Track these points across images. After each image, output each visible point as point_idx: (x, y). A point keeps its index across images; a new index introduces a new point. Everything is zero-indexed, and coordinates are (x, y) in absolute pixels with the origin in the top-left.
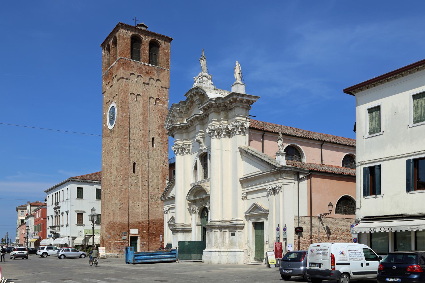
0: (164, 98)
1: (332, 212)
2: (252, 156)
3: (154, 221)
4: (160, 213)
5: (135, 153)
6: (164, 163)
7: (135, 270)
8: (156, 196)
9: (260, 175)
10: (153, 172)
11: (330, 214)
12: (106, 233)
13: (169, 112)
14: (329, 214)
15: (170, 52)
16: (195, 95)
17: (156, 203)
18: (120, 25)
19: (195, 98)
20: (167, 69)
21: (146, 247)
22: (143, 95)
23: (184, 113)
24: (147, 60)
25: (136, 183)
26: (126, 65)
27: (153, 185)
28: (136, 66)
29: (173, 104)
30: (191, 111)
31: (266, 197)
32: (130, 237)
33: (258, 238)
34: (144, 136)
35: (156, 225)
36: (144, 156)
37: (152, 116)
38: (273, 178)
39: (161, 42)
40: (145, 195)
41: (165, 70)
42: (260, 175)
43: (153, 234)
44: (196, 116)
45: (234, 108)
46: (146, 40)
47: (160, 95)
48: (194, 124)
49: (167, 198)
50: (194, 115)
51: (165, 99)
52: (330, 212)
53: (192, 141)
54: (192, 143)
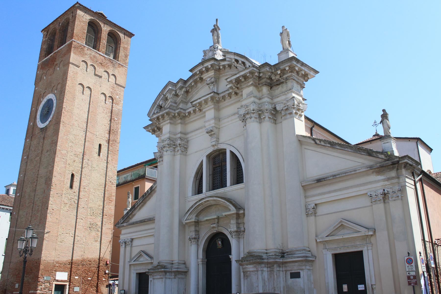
0: (118, 97)
2: (329, 146)
5: (75, 161)
6: (110, 179)
12: (11, 278)
16: (207, 70)
18: (77, 5)
19: (206, 74)
20: (124, 65)
22: (93, 89)
23: (181, 96)
24: (104, 50)
25: (72, 203)
26: (80, 49)
27: (94, 209)
28: (90, 54)
32: (54, 285)
34: (89, 140)
36: (86, 166)
37: (101, 116)
39: (122, 35)
46: (105, 29)
47: (114, 94)
48: (203, 109)
51: (119, 99)
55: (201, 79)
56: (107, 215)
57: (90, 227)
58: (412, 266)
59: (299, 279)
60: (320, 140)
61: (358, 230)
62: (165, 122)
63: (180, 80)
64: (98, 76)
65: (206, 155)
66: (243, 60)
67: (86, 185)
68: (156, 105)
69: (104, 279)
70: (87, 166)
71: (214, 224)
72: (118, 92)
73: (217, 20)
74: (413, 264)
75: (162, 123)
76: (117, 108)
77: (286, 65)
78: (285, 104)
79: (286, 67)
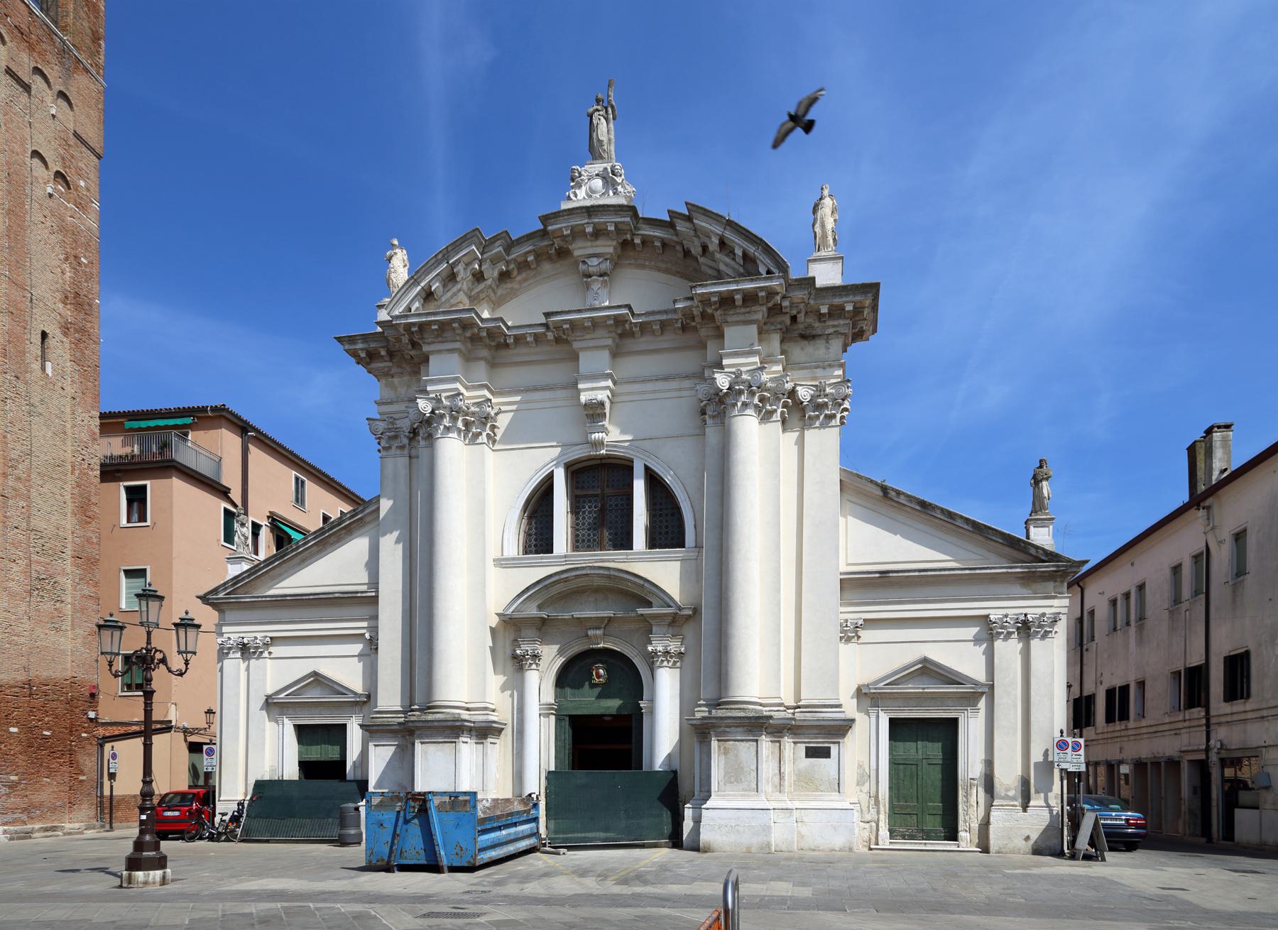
1: (212, 726)
3: (47, 687)
4: (69, 653)
6: (83, 452)
7: (1018, 869)
8: (55, 582)
9: (917, 574)
10: (46, 478)
11: (208, 730)
13: (440, 256)
14: (205, 729)
15: (103, 8)
16: (598, 233)
17: (56, 609)
19: (589, 244)
20: (94, 72)
21: (19, 795)
29: (477, 232)
30: (512, 289)
31: (973, 643)
33: (905, 768)
34: (11, 309)
35: (54, 705)
38: (1017, 589)
40: (16, 568)
41: (87, 71)
42: (917, 574)
43: (42, 739)
44: (625, 311)
45: (825, 337)
49: (254, 597)
50: (619, 307)
52: (210, 726)
53: (518, 398)
54: (514, 407)
55: (563, 253)
56: (81, 558)
57: (37, 589)
59: (828, 759)
60: (899, 493)
62: (445, 344)
63: (504, 235)
64: (15, 79)
65: (565, 461)
66: (751, 249)
67: (16, 457)
68: (419, 288)
69: (84, 735)
70: (16, 397)
71: (599, 628)
72: (80, 164)
75: (429, 343)
76: (85, 225)
77: (851, 298)
78: (820, 391)
79: (847, 302)
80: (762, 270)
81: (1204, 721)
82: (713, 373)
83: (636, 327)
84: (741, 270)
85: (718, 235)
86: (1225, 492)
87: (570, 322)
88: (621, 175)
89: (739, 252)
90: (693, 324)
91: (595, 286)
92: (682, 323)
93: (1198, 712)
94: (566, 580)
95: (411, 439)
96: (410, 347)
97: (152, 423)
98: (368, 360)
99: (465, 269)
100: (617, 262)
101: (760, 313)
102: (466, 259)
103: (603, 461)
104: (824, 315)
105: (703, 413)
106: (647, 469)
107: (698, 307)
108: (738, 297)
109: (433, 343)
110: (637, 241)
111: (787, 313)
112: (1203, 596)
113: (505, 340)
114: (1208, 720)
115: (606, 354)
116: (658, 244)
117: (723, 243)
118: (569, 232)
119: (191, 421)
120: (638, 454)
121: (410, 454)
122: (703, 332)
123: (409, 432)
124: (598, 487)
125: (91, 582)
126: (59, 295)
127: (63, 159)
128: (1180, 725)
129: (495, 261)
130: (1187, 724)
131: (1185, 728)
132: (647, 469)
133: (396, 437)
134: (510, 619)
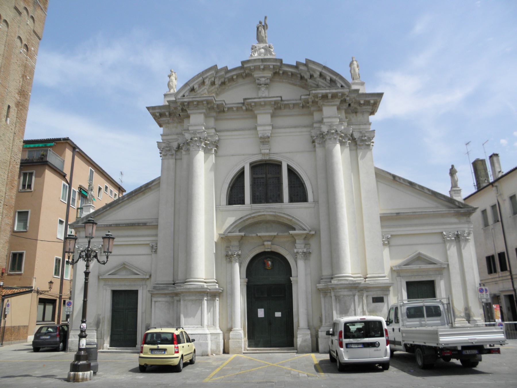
2: (409, 185)
19: (261, 72)
41: (42, 9)
58: (483, 294)
61: (428, 261)
73: (266, 18)
74: (71, 306)
75: (191, 110)
77: (373, 98)
80: (339, 85)
81: (510, 277)
82: (321, 125)
83: (282, 105)
84: (329, 85)
85: (319, 71)
86: (501, 180)
87: (255, 103)
88: (272, 48)
89: (328, 78)
90: (308, 105)
91: (263, 89)
92: (303, 105)
93: (507, 273)
94: (254, 217)
95: (176, 151)
96: (181, 111)
97: (37, 145)
98: (159, 117)
99: (208, 81)
100: (272, 80)
101: (337, 102)
102: (209, 77)
103: (267, 162)
104: (362, 104)
105: (313, 142)
106: (288, 166)
107: (311, 98)
108: (330, 96)
109: (193, 109)
110: (281, 72)
111: (348, 102)
112: (500, 223)
113: (224, 109)
114: (512, 276)
115: (269, 116)
116: (290, 74)
117: (321, 75)
118: (253, 68)
119: (53, 144)
120: (284, 159)
121: (175, 157)
122: (312, 109)
123: (176, 148)
124: (264, 174)
125: (9, 217)
126: (17, 91)
127: (28, 39)
128: (498, 279)
129: (220, 78)
130: (501, 279)
131: (500, 280)
132: (288, 166)
133: (169, 150)
134: (226, 236)
